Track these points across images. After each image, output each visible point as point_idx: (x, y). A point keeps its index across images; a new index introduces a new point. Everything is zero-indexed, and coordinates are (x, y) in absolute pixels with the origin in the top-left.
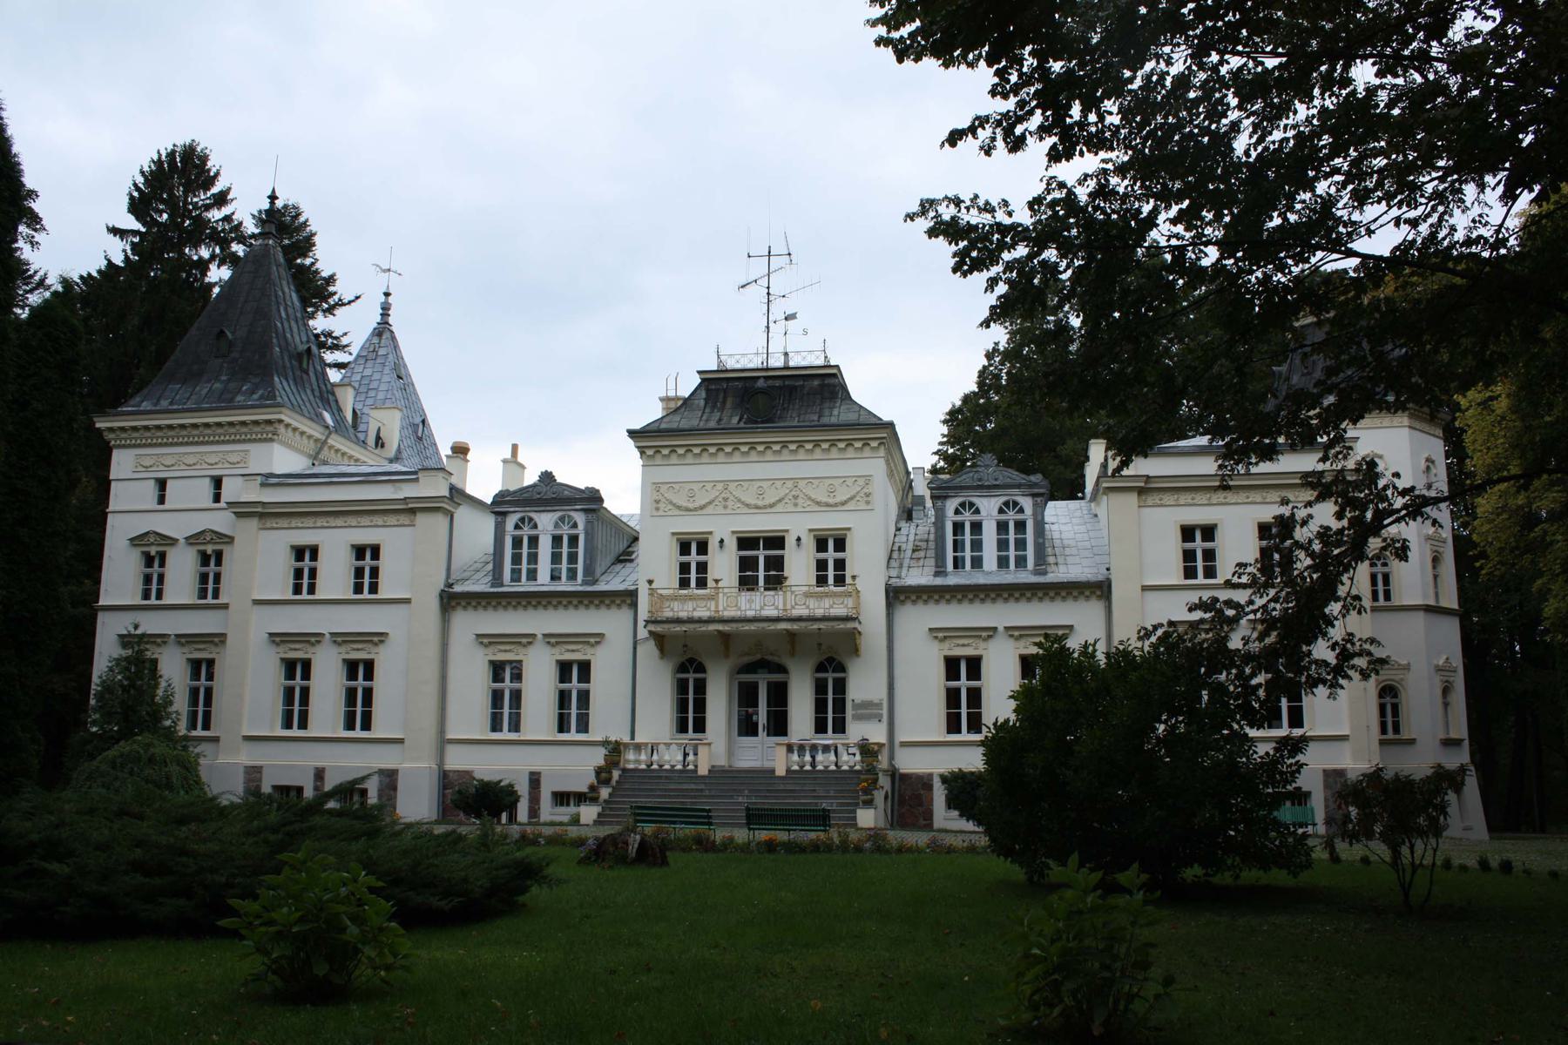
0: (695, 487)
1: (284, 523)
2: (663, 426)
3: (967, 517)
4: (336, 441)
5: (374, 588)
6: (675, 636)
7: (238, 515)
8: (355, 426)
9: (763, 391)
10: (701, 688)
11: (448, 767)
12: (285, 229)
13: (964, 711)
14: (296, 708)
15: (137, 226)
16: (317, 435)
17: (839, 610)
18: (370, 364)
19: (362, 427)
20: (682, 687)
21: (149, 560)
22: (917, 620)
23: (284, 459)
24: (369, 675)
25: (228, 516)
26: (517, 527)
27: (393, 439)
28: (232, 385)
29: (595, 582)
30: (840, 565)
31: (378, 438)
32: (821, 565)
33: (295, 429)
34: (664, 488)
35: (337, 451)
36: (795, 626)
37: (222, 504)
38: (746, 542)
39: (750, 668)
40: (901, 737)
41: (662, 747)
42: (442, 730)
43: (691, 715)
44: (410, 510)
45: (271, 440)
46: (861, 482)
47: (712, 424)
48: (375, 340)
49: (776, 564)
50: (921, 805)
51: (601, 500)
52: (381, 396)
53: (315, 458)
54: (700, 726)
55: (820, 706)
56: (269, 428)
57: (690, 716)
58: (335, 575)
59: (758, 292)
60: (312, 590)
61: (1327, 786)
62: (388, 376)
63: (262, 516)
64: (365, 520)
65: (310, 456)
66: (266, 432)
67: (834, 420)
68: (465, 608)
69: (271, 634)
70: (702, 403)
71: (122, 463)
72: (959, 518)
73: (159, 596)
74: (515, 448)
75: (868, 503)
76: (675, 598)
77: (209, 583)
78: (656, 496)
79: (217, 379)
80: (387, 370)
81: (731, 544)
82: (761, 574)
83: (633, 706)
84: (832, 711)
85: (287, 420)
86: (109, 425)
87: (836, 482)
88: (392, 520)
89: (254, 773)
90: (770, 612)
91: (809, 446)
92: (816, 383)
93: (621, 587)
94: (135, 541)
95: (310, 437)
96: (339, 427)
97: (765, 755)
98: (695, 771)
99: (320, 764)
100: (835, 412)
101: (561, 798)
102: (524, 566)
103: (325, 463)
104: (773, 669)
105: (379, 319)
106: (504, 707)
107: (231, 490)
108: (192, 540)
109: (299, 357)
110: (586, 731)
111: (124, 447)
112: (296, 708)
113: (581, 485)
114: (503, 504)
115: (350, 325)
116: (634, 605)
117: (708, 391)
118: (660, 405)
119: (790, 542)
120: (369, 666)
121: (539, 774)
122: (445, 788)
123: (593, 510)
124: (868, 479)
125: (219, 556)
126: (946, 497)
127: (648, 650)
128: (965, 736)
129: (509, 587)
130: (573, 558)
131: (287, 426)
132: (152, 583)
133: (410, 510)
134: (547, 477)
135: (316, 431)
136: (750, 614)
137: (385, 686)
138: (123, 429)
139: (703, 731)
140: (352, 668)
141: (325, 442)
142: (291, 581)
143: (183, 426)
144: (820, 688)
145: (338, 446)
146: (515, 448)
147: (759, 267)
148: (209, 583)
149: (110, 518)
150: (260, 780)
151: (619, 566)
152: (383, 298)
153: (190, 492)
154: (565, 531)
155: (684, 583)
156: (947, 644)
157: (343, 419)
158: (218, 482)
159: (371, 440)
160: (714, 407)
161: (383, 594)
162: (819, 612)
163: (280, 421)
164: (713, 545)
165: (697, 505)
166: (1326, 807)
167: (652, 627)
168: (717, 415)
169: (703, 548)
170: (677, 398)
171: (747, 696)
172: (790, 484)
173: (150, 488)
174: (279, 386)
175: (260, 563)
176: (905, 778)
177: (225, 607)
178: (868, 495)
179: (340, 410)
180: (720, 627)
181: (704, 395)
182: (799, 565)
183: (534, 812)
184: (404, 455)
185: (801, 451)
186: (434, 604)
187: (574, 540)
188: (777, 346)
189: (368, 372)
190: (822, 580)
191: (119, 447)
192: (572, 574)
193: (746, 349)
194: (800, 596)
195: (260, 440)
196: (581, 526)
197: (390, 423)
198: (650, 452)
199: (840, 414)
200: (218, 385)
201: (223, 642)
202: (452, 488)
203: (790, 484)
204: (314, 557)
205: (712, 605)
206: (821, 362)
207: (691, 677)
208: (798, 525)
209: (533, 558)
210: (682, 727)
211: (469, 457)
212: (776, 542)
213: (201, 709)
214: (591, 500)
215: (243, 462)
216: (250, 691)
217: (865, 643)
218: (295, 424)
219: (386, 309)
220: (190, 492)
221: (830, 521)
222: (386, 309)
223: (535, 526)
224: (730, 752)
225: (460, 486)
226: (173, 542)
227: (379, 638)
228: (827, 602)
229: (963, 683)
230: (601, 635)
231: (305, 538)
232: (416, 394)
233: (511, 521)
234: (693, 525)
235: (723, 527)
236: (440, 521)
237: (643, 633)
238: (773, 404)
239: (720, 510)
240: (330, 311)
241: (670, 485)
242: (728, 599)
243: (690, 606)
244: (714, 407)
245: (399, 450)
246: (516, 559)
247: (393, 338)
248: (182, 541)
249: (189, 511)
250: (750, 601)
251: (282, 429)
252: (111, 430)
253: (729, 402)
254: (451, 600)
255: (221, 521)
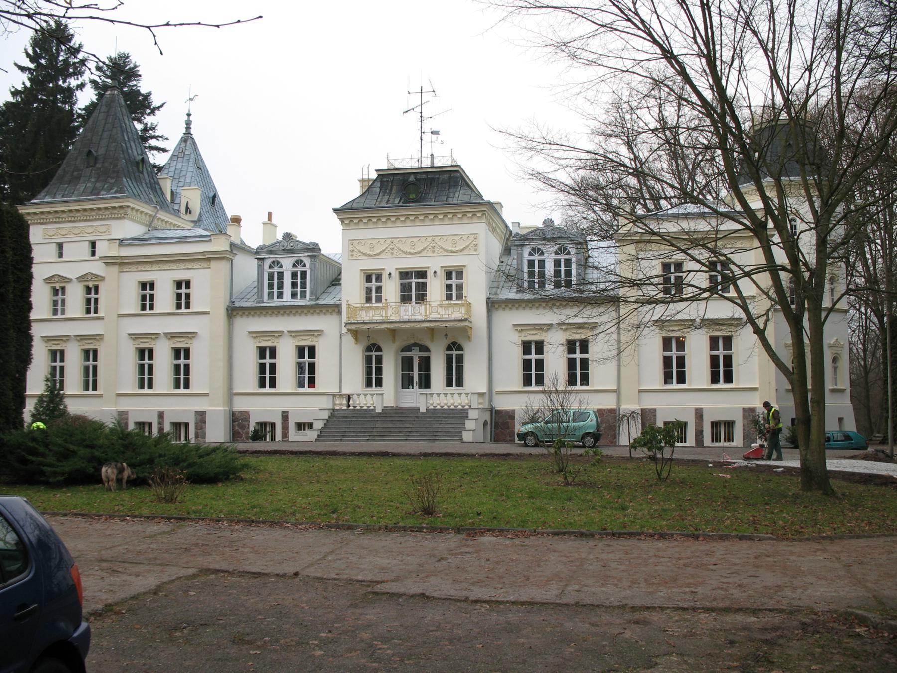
0: (374, 242)
1: (133, 268)
2: (355, 206)
3: (536, 257)
4: (162, 215)
5: (188, 306)
6: (363, 331)
7: (107, 264)
8: (173, 201)
9: (412, 184)
10: (379, 360)
11: (235, 409)
12: (121, 71)
13: (533, 373)
14: (146, 377)
15: (32, 66)
16: (150, 213)
17: (457, 315)
18: (180, 160)
19: (177, 201)
20: (368, 360)
21: (56, 292)
22: (507, 320)
23: (129, 229)
24: (187, 357)
25: (101, 264)
26: (270, 267)
27: (196, 207)
28: (98, 185)
29: (318, 299)
30: (460, 287)
31: (187, 208)
32: (449, 287)
33: (137, 210)
34: (356, 243)
35: (163, 220)
36: (432, 325)
37: (96, 257)
38: (404, 274)
39: (408, 349)
40: (497, 388)
41: (355, 397)
42: (230, 386)
43: (374, 377)
44: (207, 259)
45: (123, 218)
46: (472, 237)
47: (383, 204)
48: (183, 145)
49: (422, 287)
50: (508, 428)
51: (320, 250)
52: (188, 181)
53: (151, 227)
54: (379, 383)
55: (449, 370)
56: (122, 211)
57: (374, 377)
58: (165, 298)
59: (414, 116)
60: (152, 307)
61: (744, 417)
62: (192, 168)
63: (121, 264)
64: (182, 266)
65: (146, 225)
66: (120, 213)
67: (455, 201)
68: (241, 316)
69: (129, 334)
70: (378, 190)
71: (36, 234)
72: (531, 258)
73: (63, 313)
74: (270, 214)
75: (476, 250)
76: (363, 308)
77: (91, 306)
78: (352, 249)
79: (89, 181)
80: (191, 164)
81: (395, 275)
82: (414, 293)
83: (341, 373)
84: (455, 375)
85: (132, 206)
86: (27, 211)
87: (457, 238)
88: (197, 265)
89: (123, 416)
90: (418, 317)
91: (440, 217)
92: (446, 176)
93: (332, 302)
94: (48, 280)
95: (146, 214)
96: (163, 205)
97: (415, 399)
98: (374, 410)
99: (161, 409)
100: (457, 195)
101: (301, 426)
102: (276, 290)
103: (156, 229)
104: (418, 353)
105: (184, 131)
106: (267, 376)
107: (102, 249)
108: (81, 279)
109: (137, 163)
110: (314, 387)
111: (37, 224)
112: (146, 377)
113: (307, 241)
114: (260, 254)
115: (166, 126)
116: (340, 313)
117: (382, 182)
118: (358, 185)
119: (430, 274)
120: (187, 352)
121: (126, 413)
122: (233, 421)
123: (315, 256)
124: (476, 236)
125: (97, 288)
126: (523, 245)
127: (349, 339)
128: (534, 388)
129: (266, 302)
130: (304, 285)
131: (133, 209)
132: (57, 306)
133: (207, 259)
134: (288, 236)
135: (148, 210)
136: (406, 318)
137: (198, 364)
138: (35, 214)
139: (381, 386)
140: (177, 353)
141: (155, 217)
142: (140, 302)
143: (70, 211)
144: (449, 360)
145: (163, 218)
146: (270, 214)
147: (415, 100)
148: (91, 306)
149: (34, 265)
150: (127, 419)
151: (332, 288)
152: (186, 118)
153: (77, 250)
154: (299, 269)
155: (368, 299)
156: (524, 334)
157: (165, 199)
158: (93, 245)
159: (183, 210)
160: (385, 193)
161: (193, 309)
162: (446, 317)
163: (128, 207)
164: (385, 276)
165: (375, 253)
166: (744, 430)
167: (349, 327)
168: (386, 197)
169: (379, 278)
170: (369, 180)
171: (407, 364)
172: (429, 240)
173: (54, 248)
174: (126, 184)
175: (120, 293)
176: (498, 412)
177: (102, 318)
178: (476, 245)
179: (163, 194)
180: (389, 326)
181: (379, 185)
182: (435, 288)
183: (285, 434)
184: (204, 218)
185: (436, 219)
186: (221, 313)
187: (304, 274)
188: (426, 152)
189: (179, 166)
190: (449, 297)
191: (34, 224)
192: (304, 295)
193: (407, 156)
194: (435, 307)
195: (117, 218)
196: (308, 266)
197: (192, 197)
198: (347, 222)
199: (461, 195)
200: (89, 185)
201: (102, 339)
202: (232, 245)
203: (429, 240)
204: (152, 288)
205: (383, 312)
206: (449, 163)
207: (374, 354)
208: (434, 264)
209: (281, 286)
210: (369, 384)
211: (242, 223)
212: (422, 274)
213: (91, 378)
214: (314, 249)
215: (108, 231)
216: (117, 368)
217: (474, 334)
218: (137, 207)
219: (188, 124)
220: (77, 250)
221: (452, 262)
222: (188, 124)
223: (281, 266)
224: (397, 397)
225: (238, 242)
226: (69, 280)
227: (192, 335)
228: (450, 310)
229: (533, 357)
230: (321, 331)
231: (147, 277)
232: (209, 177)
233: (267, 263)
234: (373, 265)
235: (391, 265)
236: (224, 266)
237: (344, 330)
238: (421, 189)
239: (389, 256)
240: (153, 111)
241: (360, 241)
242: (391, 309)
243: (371, 313)
244: (385, 193)
245: (200, 215)
246: (271, 286)
247: (194, 143)
248: (74, 280)
249: (76, 264)
250: (406, 310)
251: (129, 211)
252: (28, 214)
253: (394, 188)
254: (233, 311)
255: (97, 268)
